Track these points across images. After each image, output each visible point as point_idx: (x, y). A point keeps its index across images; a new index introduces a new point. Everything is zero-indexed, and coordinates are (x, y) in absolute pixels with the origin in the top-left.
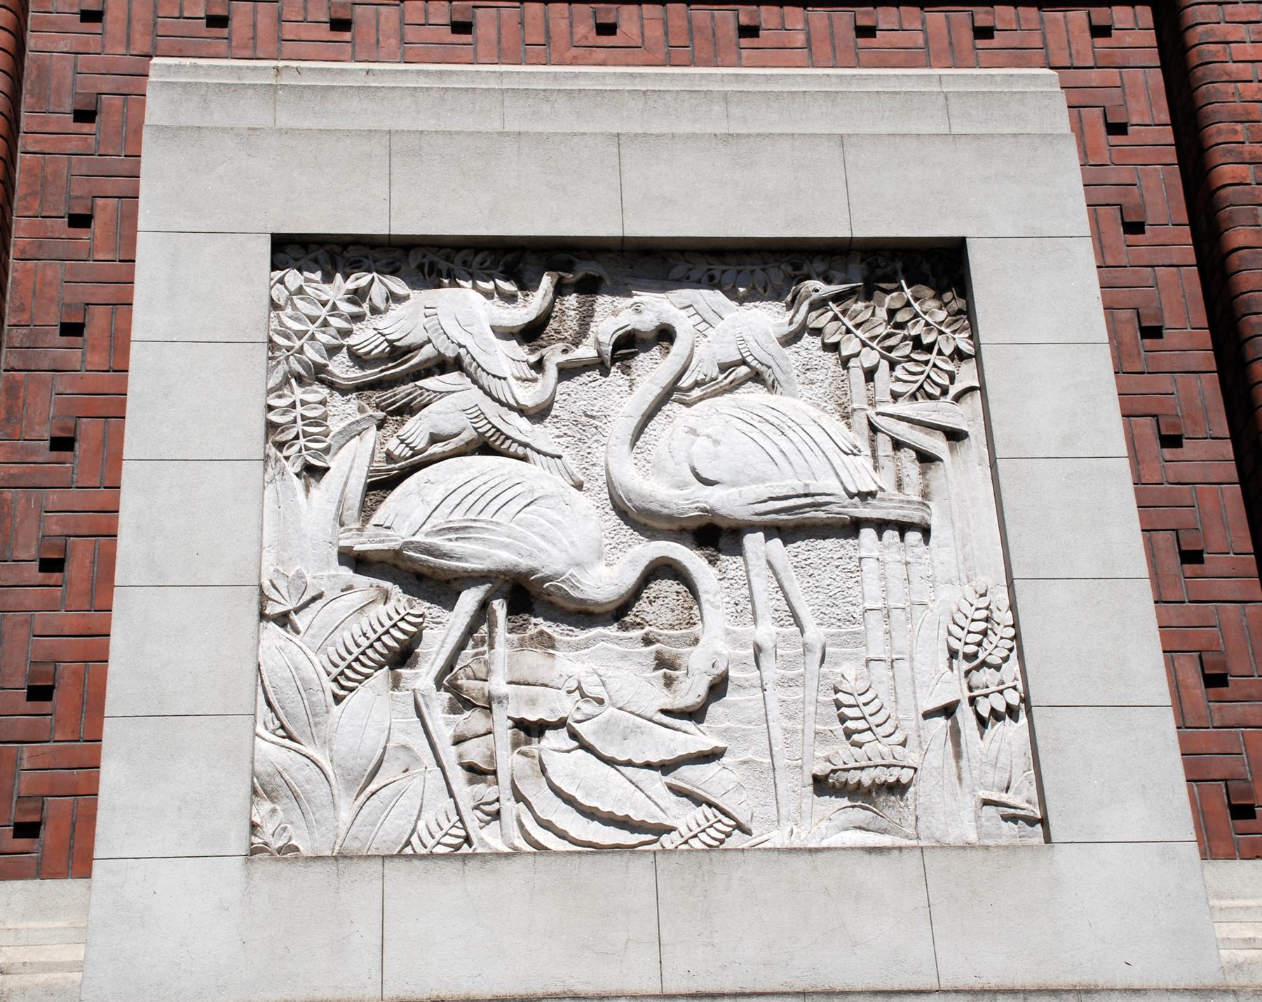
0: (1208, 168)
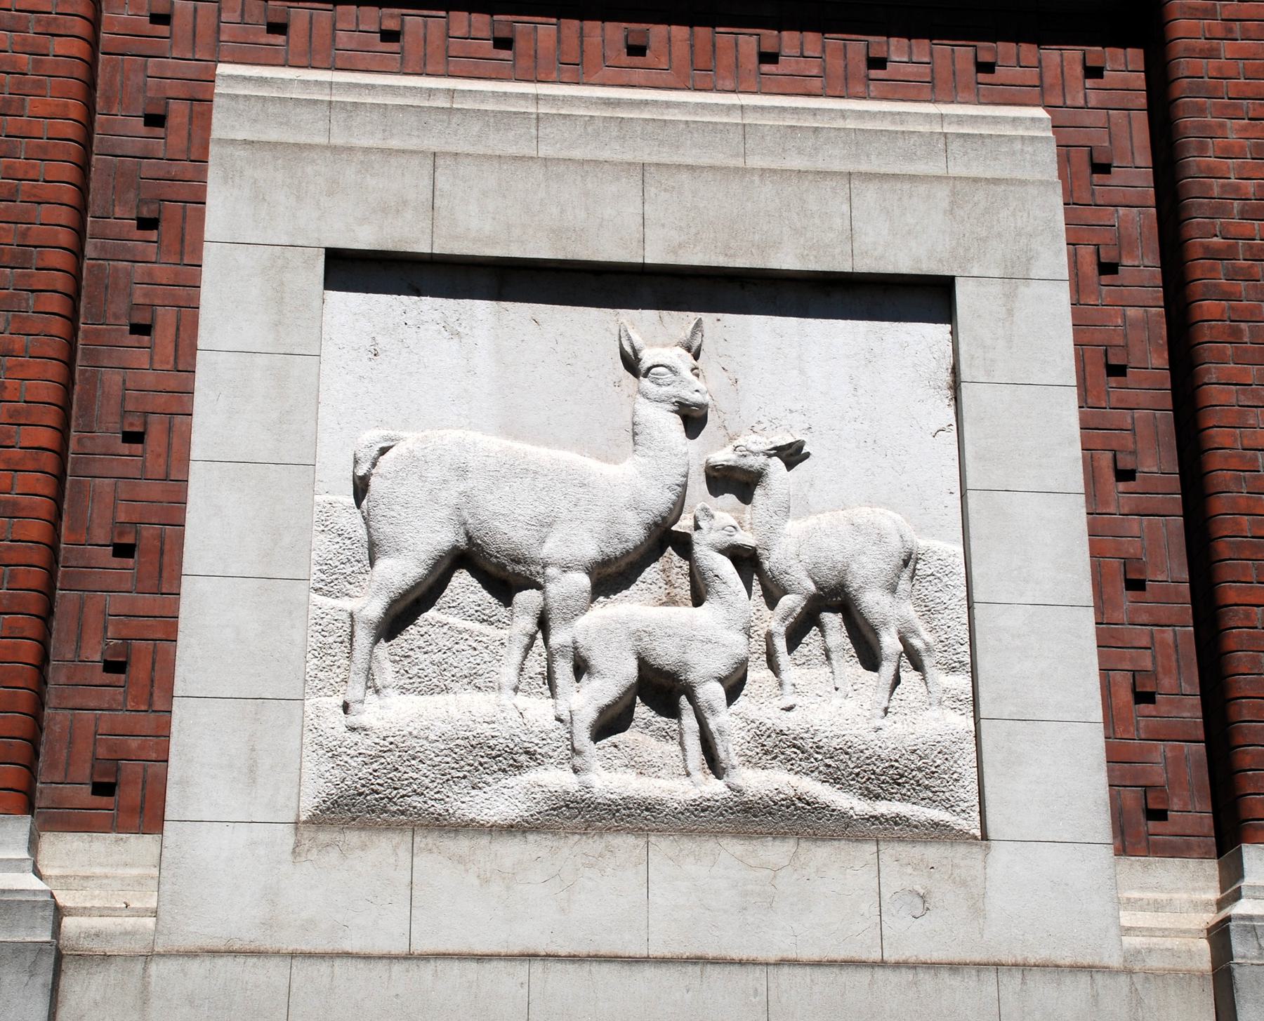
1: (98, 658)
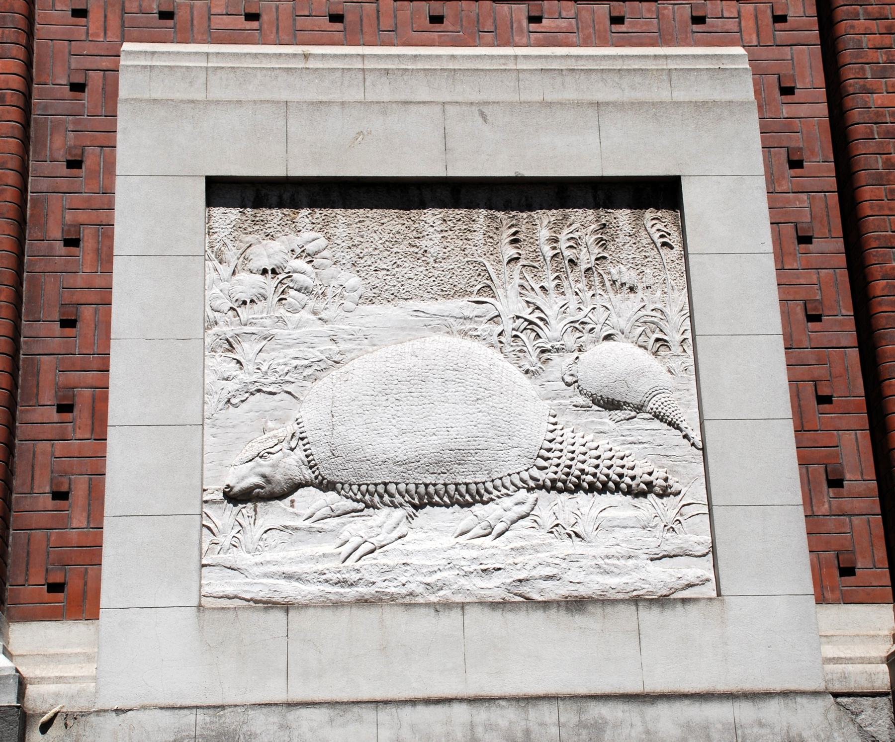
0: (839, 66)
1: (48, 489)
